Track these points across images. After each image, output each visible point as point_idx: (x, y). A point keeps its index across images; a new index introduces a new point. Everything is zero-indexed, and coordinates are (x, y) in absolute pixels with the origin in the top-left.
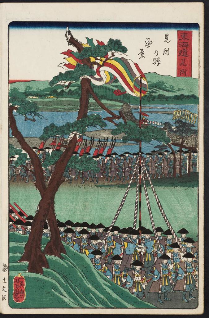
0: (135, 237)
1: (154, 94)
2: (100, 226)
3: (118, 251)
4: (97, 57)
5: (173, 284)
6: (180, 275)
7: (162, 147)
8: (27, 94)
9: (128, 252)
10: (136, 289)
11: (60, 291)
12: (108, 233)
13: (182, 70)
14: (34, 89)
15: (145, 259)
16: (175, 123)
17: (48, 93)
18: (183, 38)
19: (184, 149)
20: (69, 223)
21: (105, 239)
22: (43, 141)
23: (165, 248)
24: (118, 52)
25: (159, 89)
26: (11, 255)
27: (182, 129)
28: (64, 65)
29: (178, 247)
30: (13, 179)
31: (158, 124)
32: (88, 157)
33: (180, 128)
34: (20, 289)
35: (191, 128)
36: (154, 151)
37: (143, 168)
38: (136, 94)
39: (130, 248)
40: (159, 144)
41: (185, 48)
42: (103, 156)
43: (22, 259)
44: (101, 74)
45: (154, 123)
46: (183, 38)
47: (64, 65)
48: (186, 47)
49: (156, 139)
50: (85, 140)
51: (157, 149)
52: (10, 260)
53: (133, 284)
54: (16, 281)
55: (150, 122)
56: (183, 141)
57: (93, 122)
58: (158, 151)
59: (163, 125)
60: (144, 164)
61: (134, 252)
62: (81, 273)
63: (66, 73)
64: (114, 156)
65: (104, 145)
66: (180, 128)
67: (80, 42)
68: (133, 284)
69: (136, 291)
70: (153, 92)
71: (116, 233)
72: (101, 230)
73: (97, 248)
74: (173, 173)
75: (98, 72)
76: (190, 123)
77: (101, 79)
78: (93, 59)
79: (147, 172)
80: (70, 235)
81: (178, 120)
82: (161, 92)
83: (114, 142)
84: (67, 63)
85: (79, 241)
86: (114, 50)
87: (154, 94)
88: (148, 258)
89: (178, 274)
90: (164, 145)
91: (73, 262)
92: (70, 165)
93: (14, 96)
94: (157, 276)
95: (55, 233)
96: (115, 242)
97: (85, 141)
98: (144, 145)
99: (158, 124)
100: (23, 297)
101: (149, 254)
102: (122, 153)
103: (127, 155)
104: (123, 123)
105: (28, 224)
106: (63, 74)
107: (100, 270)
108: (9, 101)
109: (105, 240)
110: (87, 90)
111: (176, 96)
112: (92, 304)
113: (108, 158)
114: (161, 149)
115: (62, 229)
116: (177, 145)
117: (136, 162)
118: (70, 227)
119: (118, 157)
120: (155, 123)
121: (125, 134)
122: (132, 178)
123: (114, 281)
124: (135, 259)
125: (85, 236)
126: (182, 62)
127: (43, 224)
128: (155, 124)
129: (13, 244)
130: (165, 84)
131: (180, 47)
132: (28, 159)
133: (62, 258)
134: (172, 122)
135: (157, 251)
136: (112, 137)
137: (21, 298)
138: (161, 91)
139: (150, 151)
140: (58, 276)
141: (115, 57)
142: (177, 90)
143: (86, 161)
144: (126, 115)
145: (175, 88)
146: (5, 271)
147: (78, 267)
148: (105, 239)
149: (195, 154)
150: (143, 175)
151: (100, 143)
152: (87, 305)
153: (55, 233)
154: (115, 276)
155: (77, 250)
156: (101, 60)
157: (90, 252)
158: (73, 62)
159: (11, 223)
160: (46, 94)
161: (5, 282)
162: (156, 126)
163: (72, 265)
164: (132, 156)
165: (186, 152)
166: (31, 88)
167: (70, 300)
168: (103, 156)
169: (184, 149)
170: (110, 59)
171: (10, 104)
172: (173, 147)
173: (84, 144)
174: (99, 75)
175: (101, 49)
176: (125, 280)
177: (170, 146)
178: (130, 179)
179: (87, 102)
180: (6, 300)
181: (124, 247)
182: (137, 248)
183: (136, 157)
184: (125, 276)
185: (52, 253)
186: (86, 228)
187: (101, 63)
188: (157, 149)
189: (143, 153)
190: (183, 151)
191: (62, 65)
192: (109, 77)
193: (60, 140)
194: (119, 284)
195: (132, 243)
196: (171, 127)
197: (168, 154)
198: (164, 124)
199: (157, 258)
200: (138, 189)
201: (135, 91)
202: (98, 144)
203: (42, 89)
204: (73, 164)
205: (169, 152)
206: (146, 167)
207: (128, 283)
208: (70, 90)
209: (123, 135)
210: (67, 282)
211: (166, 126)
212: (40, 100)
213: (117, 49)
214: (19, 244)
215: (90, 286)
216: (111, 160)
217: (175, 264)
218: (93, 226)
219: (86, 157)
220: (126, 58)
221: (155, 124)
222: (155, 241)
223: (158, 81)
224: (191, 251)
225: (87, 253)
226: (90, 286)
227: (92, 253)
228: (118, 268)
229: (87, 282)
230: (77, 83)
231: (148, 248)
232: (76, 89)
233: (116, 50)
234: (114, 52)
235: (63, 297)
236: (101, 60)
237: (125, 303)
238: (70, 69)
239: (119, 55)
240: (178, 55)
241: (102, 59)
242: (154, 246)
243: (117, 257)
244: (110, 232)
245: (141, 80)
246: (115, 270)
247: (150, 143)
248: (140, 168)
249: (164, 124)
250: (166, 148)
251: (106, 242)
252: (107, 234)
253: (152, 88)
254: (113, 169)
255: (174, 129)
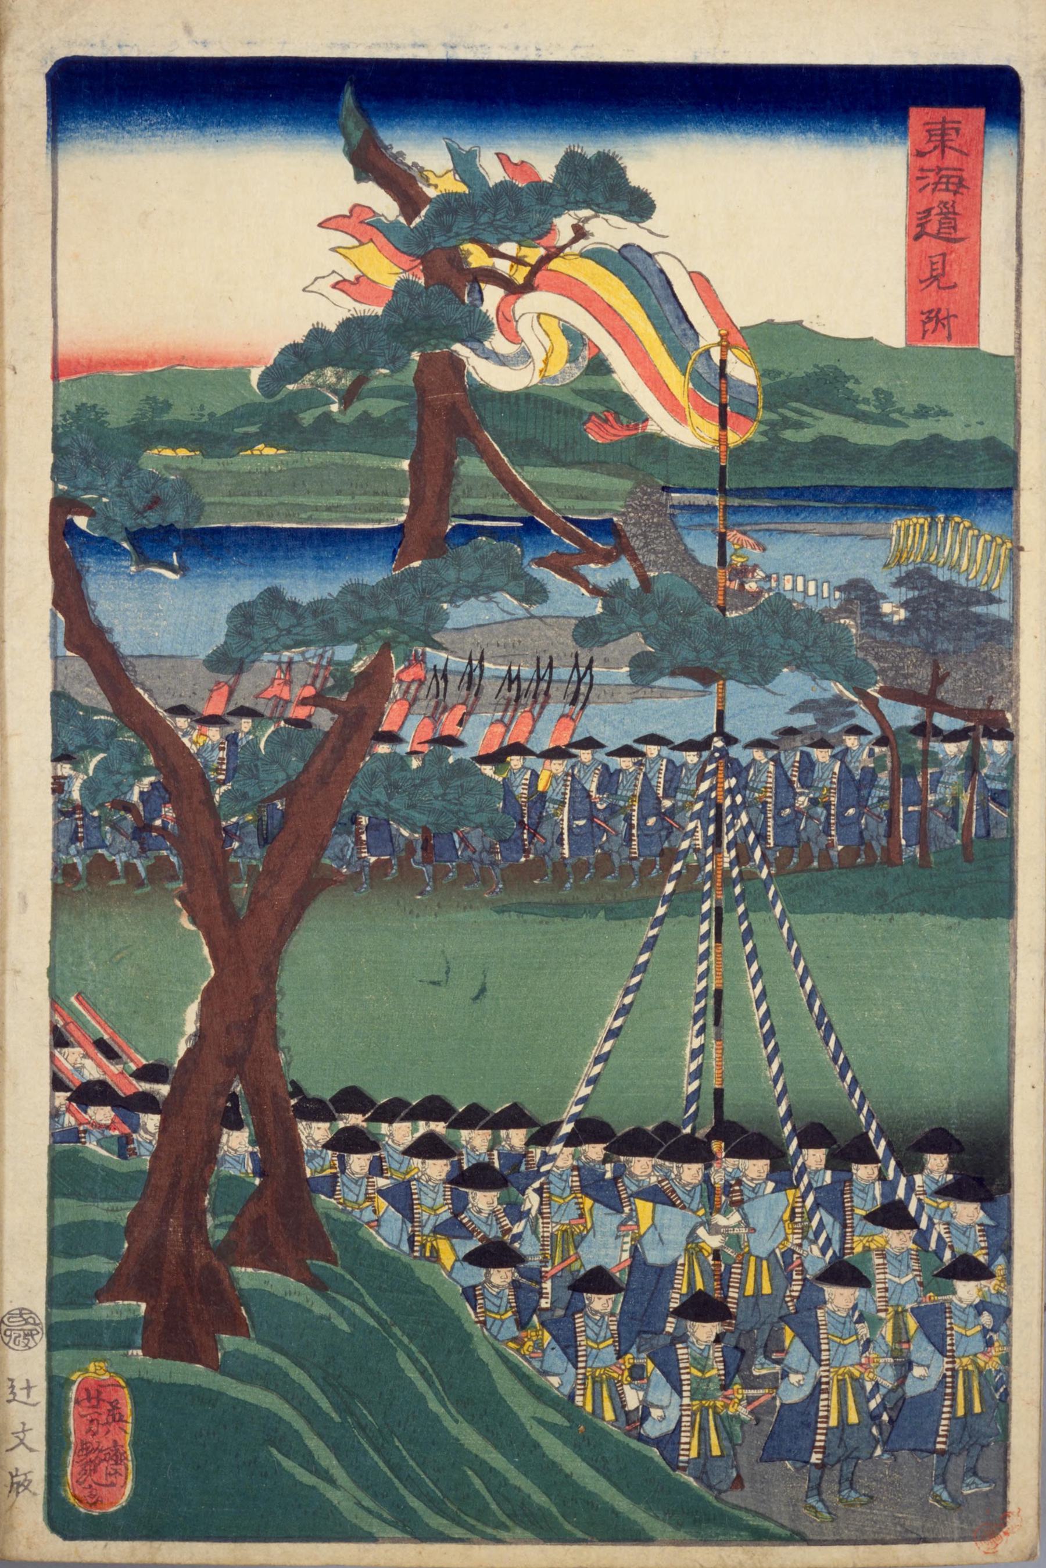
0: (691, 1172)
1: (789, 434)
2: (514, 1117)
3: (606, 1250)
4: (500, 242)
5: (885, 1417)
6: (917, 1371)
7: (829, 710)
8: (147, 432)
9: (654, 1256)
10: (695, 1442)
11: (310, 1453)
12: (554, 1158)
13: (930, 312)
14: (181, 412)
15: (742, 1287)
16: (899, 583)
17: (253, 429)
18: (935, 148)
19: (943, 721)
20: (352, 1099)
21: (536, 1185)
22: (223, 678)
23: (844, 1226)
24: (607, 216)
25: (816, 407)
26: (64, 1265)
27: (931, 616)
28: (334, 286)
29: (911, 1223)
30: (76, 884)
31: (812, 591)
32: (451, 760)
33: (923, 613)
34: (106, 1444)
35: (979, 609)
36: (790, 732)
37: (733, 818)
38: (696, 433)
39: (666, 1235)
40: (816, 694)
41: (946, 196)
42: (531, 753)
43: (114, 1288)
44: (524, 328)
45: (789, 586)
46: (935, 148)
47: (334, 286)
48: (955, 193)
49: (800, 663)
50: (435, 668)
51: (806, 720)
52: (61, 1291)
53: (679, 1422)
54: (89, 1399)
55: (768, 578)
56: (938, 680)
57: (481, 579)
58: (812, 727)
59: (837, 594)
60: (739, 799)
61: (686, 1250)
62: (415, 1361)
63: (347, 324)
64: (585, 755)
65: (535, 697)
66: (923, 613)
67: (415, 164)
68: (679, 1422)
69: (694, 1454)
70: (787, 423)
71: (595, 1151)
72: (517, 1138)
73: (494, 1233)
74: (884, 842)
75: (508, 324)
76: (971, 585)
77: (525, 356)
78: (477, 257)
79: (751, 837)
80: (359, 1163)
81: (911, 567)
82: (829, 424)
83: (587, 679)
84: (350, 274)
85: (402, 1197)
86: (588, 206)
87: (789, 434)
88: (756, 1281)
89: (909, 1365)
90: (838, 701)
91: (377, 1309)
92: (362, 798)
93: (84, 444)
94: (800, 1377)
95: (279, 1153)
96: (588, 1203)
97: (435, 676)
98: (739, 695)
99: (812, 591)
100: (120, 1480)
101: (761, 1259)
102: (629, 742)
103: (652, 750)
104: (634, 583)
105: (147, 1103)
106: (329, 332)
107: (511, 1345)
108: (57, 472)
109: (539, 1191)
110: (450, 417)
111: (906, 443)
112: (472, 1522)
113: (558, 766)
114: (826, 721)
115: (315, 1133)
116: (909, 697)
117: (698, 785)
118: (355, 1119)
119: (606, 760)
120: (795, 582)
121: (645, 638)
122: (677, 867)
123: (584, 1402)
124: (691, 1283)
125: (437, 1169)
126: (933, 270)
127: (223, 1103)
128: (794, 589)
129: (73, 1211)
130: (850, 385)
131: (920, 190)
132: (149, 767)
133: (318, 1284)
134: (881, 581)
135: (800, 1245)
136: (577, 656)
137: (113, 1485)
138: (828, 417)
139: (770, 731)
140: (297, 1374)
141: (592, 240)
142: (909, 416)
143: (444, 781)
144: (646, 545)
145: (898, 406)
146: (32, 1344)
147: (396, 1330)
148: (536, 1185)
149: (999, 747)
150: (733, 853)
151: (515, 686)
152: (436, 1522)
153: (279, 1153)
154: (586, 1378)
155: (396, 1243)
156: (518, 261)
157: (461, 1255)
158: (386, 271)
159: (61, 1097)
160: (246, 434)
161: (30, 1401)
162: (799, 598)
163: (372, 1322)
164: (678, 757)
165: (954, 737)
166: (167, 406)
167: (359, 1503)
168: (531, 753)
169: (943, 721)
170: (567, 250)
171: (61, 487)
172: (887, 706)
173: (433, 691)
174: (514, 337)
175: (519, 210)
176: (641, 1394)
177: (872, 705)
178: (665, 875)
179: (449, 474)
180: (31, 1450)
181: (637, 1224)
182: (701, 1232)
183: (696, 759)
184: (637, 1374)
185: (267, 1260)
186: (439, 1127)
187: (520, 275)
188: (806, 720)
189: (736, 741)
190: (937, 732)
191: (324, 286)
192: (562, 345)
193: (313, 670)
194: (609, 1415)
195: (674, 1205)
196: (878, 607)
197: (861, 745)
198: (839, 589)
199: (804, 1280)
200: (704, 927)
201: (696, 418)
202: (504, 691)
203: (220, 413)
204: (379, 794)
205: (870, 733)
206: (748, 813)
207: (656, 1413)
208: (366, 415)
209: (635, 643)
210: (343, 1409)
211: (849, 601)
212: (211, 465)
213: (601, 200)
214: (99, 1212)
215: (472, 1440)
216: (573, 776)
217: (897, 1313)
218: (474, 1117)
219: (442, 759)
220: (650, 244)
221: (794, 589)
222: (791, 1193)
223: (816, 366)
224: (972, 1242)
225: (448, 1258)
226: (472, 1440)
227: (475, 1258)
228: (602, 1334)
229: (449, 1413)
230: (399, 376)
231: (754, 1230)
232: (396, 409)
233: (600, 208)
234: (587, 219)
235: (322, 1486)
236: (518, 261)
237: (640, 1516)
238: (367, 307)
239: (610, 231)
240: (913, 234)
241: (525, 251)
242: (786, 1216)
243: (598, 1280)
244: (565, 1146)
245: (723, 362)
246: (590, 1343)
247: (768, 686)
248: (718, 819)
249: (839, 589)
250: (852, 715)
251: (541, 1204)
252: (546, 1158)
253: (784, 405)
254: (582, 823)
255: (893, 613)
